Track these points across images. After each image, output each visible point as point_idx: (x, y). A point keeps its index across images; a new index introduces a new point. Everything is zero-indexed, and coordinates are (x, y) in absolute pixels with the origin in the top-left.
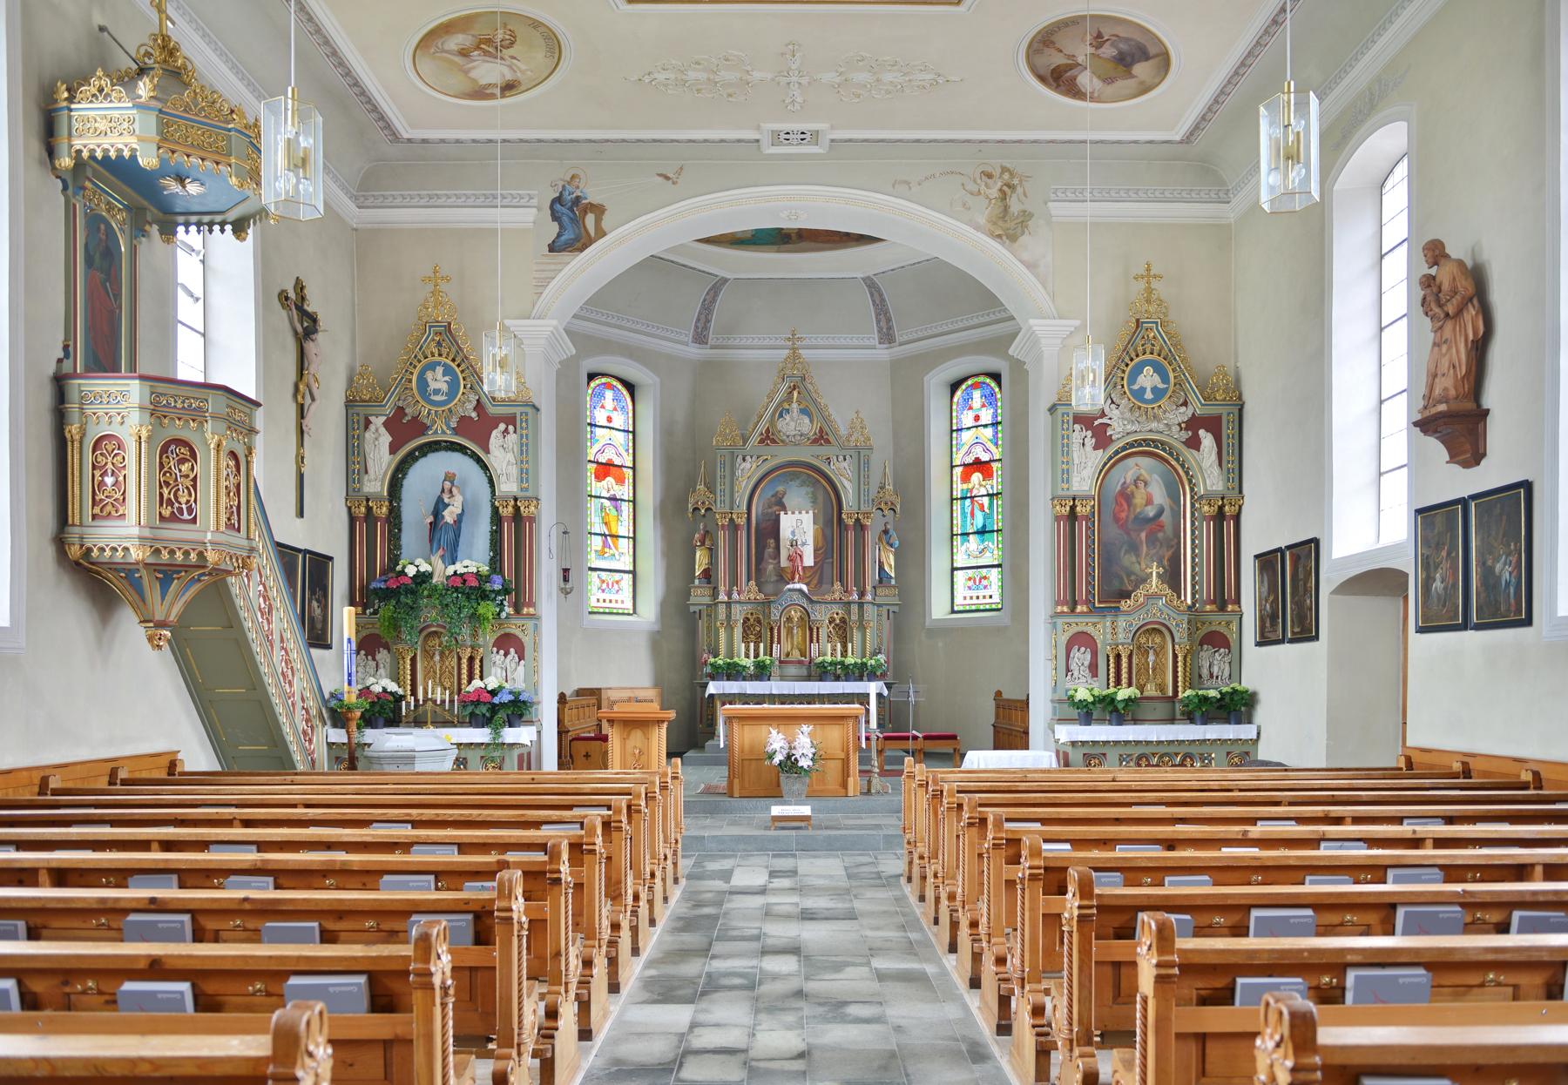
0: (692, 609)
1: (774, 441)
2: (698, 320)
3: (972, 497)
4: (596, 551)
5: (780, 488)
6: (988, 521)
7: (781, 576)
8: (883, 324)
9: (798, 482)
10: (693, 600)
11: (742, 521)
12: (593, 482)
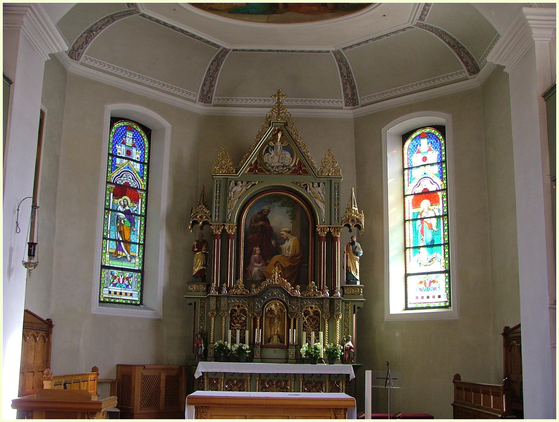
0: (189, 301)
1: (261, 171)
2: (204, 84)
3: (422, 219)
4: (110, 253)
5: (265, 207)
8: (349, 91)
9: (279, 204)
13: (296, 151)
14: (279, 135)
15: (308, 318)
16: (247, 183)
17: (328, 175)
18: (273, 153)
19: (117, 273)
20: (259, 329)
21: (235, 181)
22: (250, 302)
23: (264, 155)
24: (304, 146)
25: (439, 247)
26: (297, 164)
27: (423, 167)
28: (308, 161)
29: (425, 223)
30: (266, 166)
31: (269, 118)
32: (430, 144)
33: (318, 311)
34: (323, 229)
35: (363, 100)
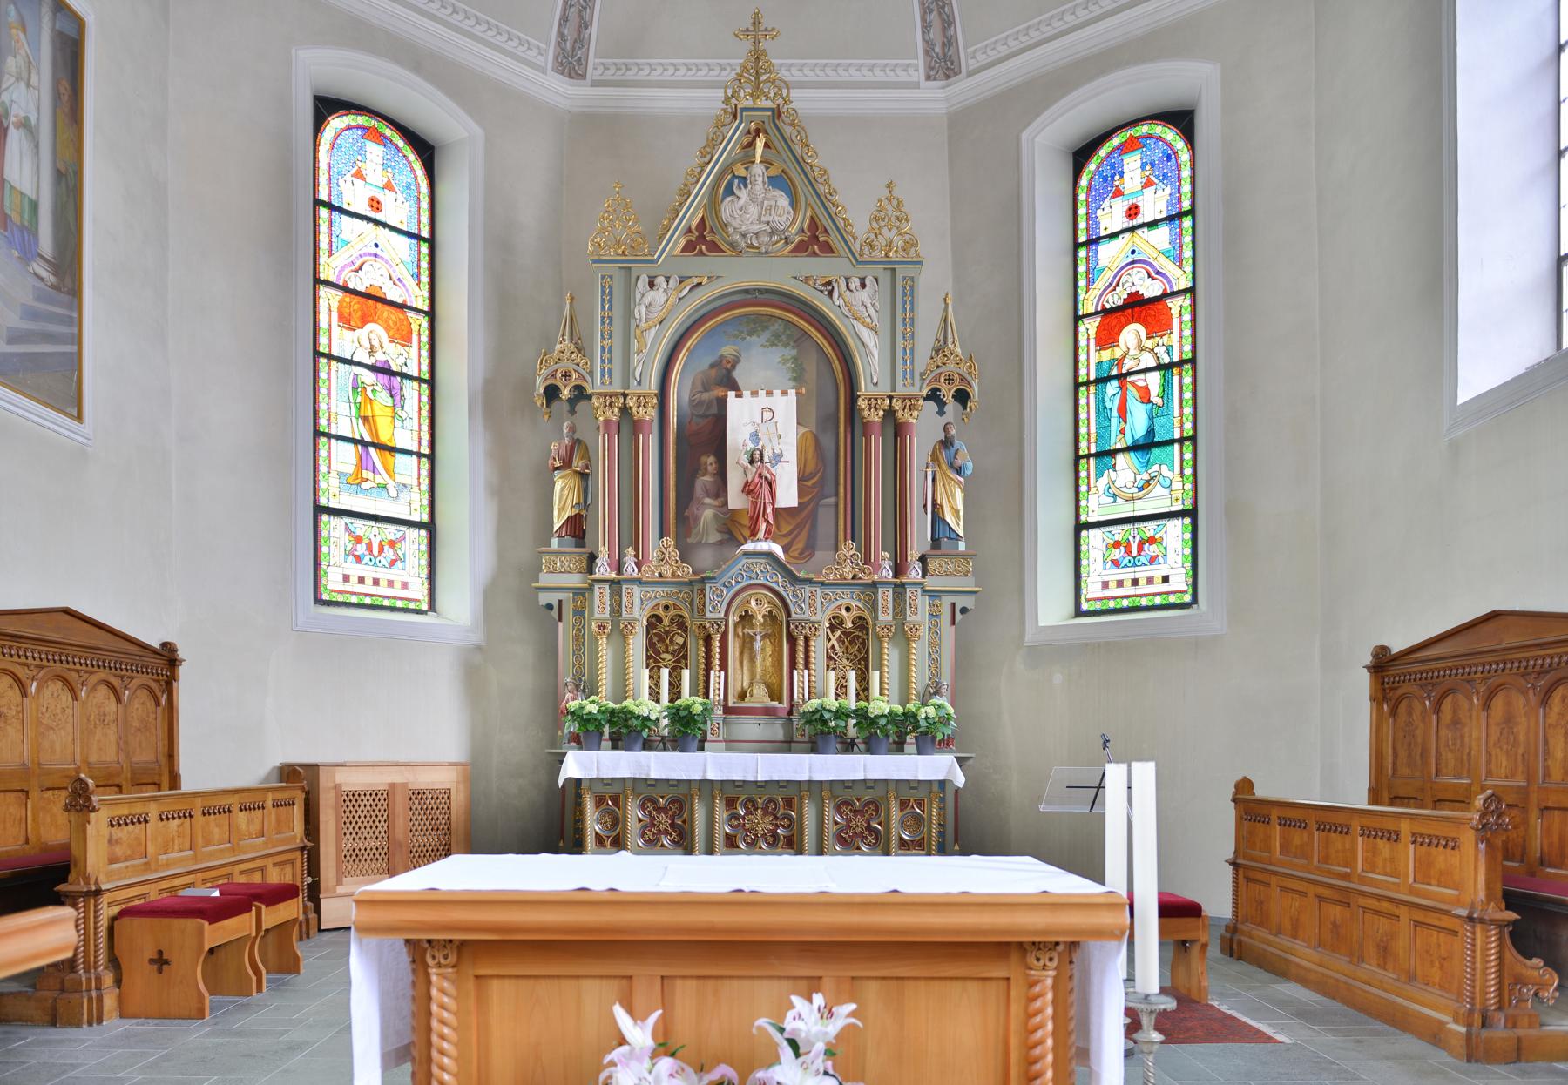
0: (545, 598)
1: (714, 248)
2: (564, 20)
3: (1121, 377)
4: (340, 474)
5: (728, 350)
6: (1158, 422)
7: (730, 533)
8: (936, 34)
9: (765, 336)
10: (546, 579)
11: (649, 414)
12: (336, 330)
13: (804, 188)
14: (760, 144)
15: (840, 636)
16: (680, 282)
17: (887, 256)
18: (743, 194)
19: (362, 526)
20: (720, 671)
21: (649, 277)
22: (695, 595)
23: (722, 202)
25: (1168, 449)
26: (805, 226)
27: (1127, 236)
28: (834, 216)
29: (1130, 386)
30: (727, 233)
31: (733, 96)
32: (1148, 168)
33: (864, 619)
34: (873, 402)
35: (974, 58)
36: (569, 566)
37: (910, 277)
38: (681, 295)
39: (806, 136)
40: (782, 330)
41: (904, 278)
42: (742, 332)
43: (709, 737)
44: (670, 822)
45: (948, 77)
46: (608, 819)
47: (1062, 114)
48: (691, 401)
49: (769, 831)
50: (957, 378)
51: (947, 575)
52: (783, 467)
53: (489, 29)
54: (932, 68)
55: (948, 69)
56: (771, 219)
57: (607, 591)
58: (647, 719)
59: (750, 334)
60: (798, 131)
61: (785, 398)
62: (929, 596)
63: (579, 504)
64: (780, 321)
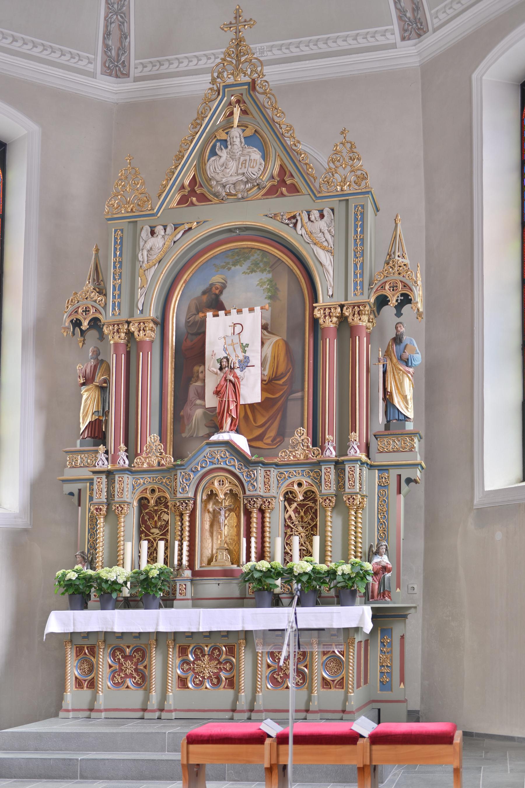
0: (68, 488)
1: (203, 198)
2: (107, 34)
5: (217, 279)
14: (237, 112)
15: (296, 508)
16: (175, 229)
17: (342, 190)
18: (224, 154)
21: (150, 227)
24: (290, 130)
30: (211, 186)
31: (218, 77)
34: (327, 311)
35: (437, 17)
36: (87, 462)
37: (360, 205)
38: (176, 239)
39: (276, 102)
40: (260, 259)
41: (356, 206)
42: (228, 263)
43: (178, 596)
44: (134, 667)
45: (419, 36)
46: (86, 666)
47: (503, 53)
48: (187, 322)
49: (214, 674)
50: (400, 286)
51: (394, 451)
52: (249, 371)
53: (45, 49)
54: (405, 31)
55: (419, 29)
56: (245, 171)
57: (333, 471)
58: (115, 583)
59: (234, 265)
60: (269, 98)
61: (252, 314)
62: (378, 470)
63: (98, 411)
64: (258, 252)
